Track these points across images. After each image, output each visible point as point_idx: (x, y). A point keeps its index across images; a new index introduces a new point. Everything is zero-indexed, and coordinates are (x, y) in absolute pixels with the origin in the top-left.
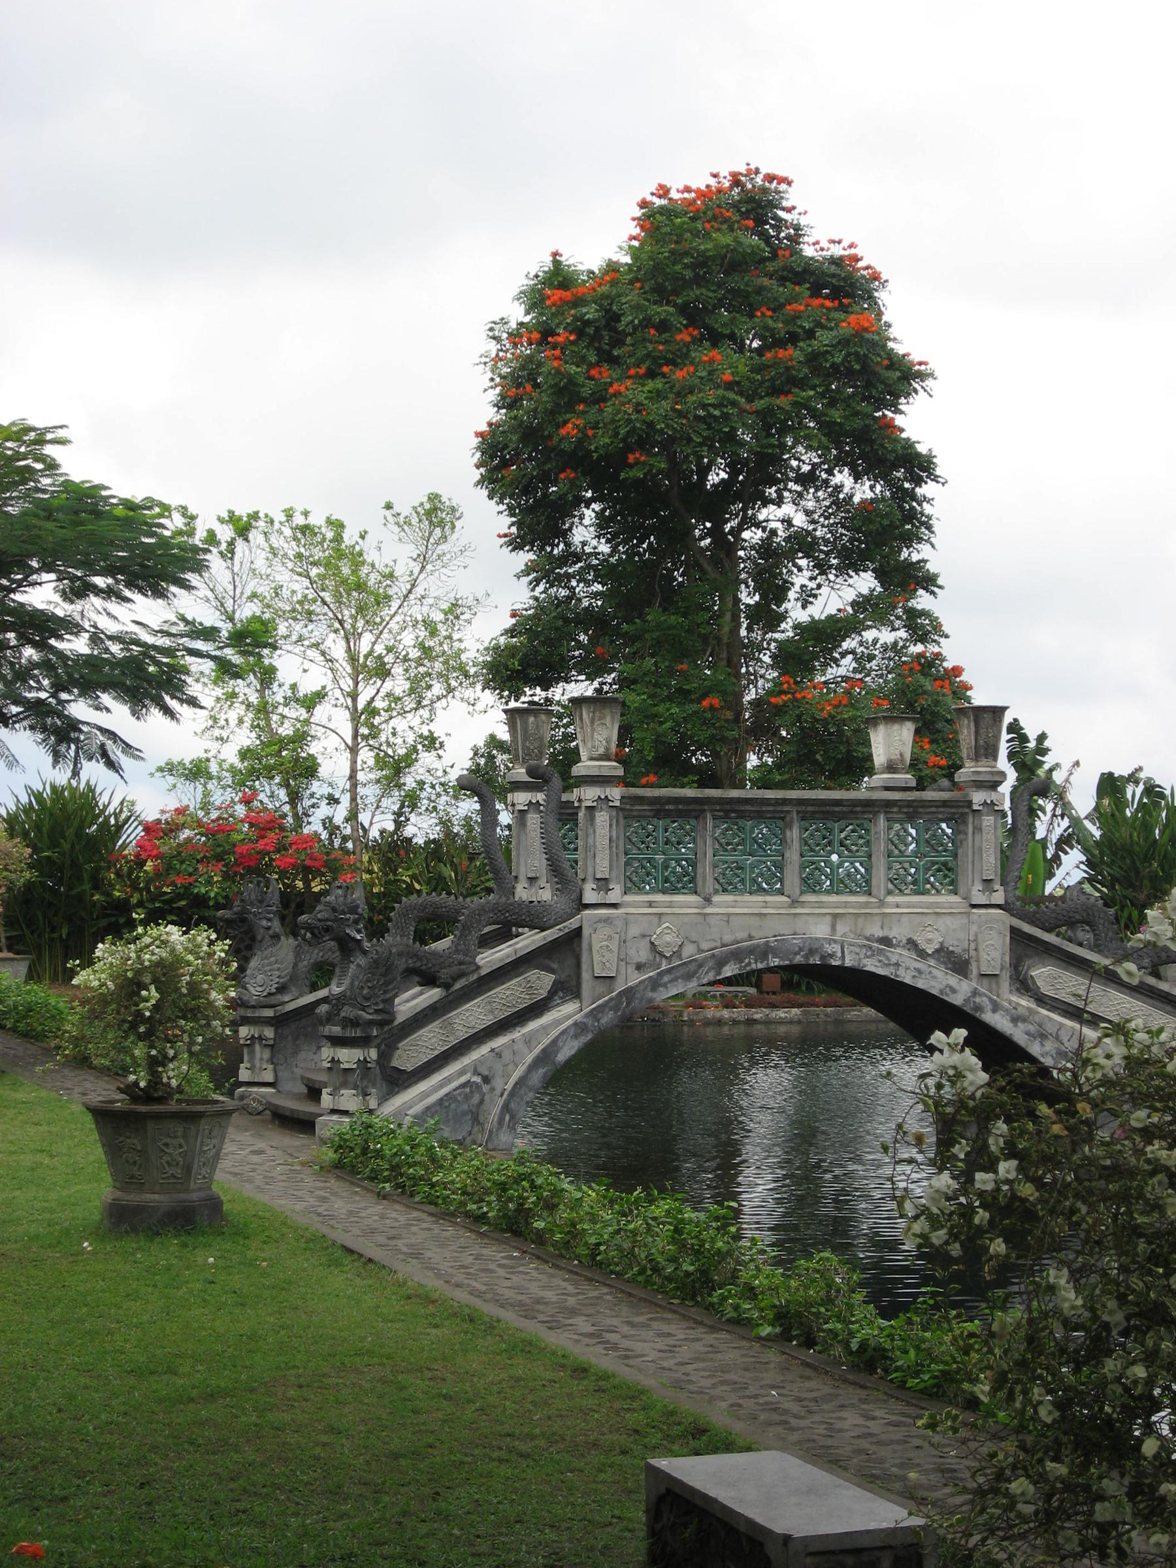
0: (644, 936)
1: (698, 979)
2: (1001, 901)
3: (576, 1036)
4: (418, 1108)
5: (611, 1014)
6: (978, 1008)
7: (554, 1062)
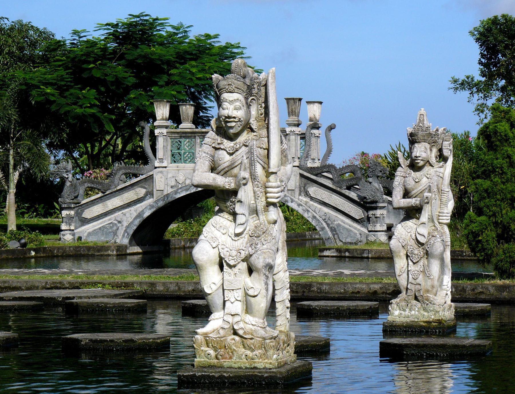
0: (173, 177)
1: (190, 191)
2: (298, 165)
3: (150, 209)
4: (91, 230)
5: (162, 202)
6: (287, 201)
7: (143, 217)
